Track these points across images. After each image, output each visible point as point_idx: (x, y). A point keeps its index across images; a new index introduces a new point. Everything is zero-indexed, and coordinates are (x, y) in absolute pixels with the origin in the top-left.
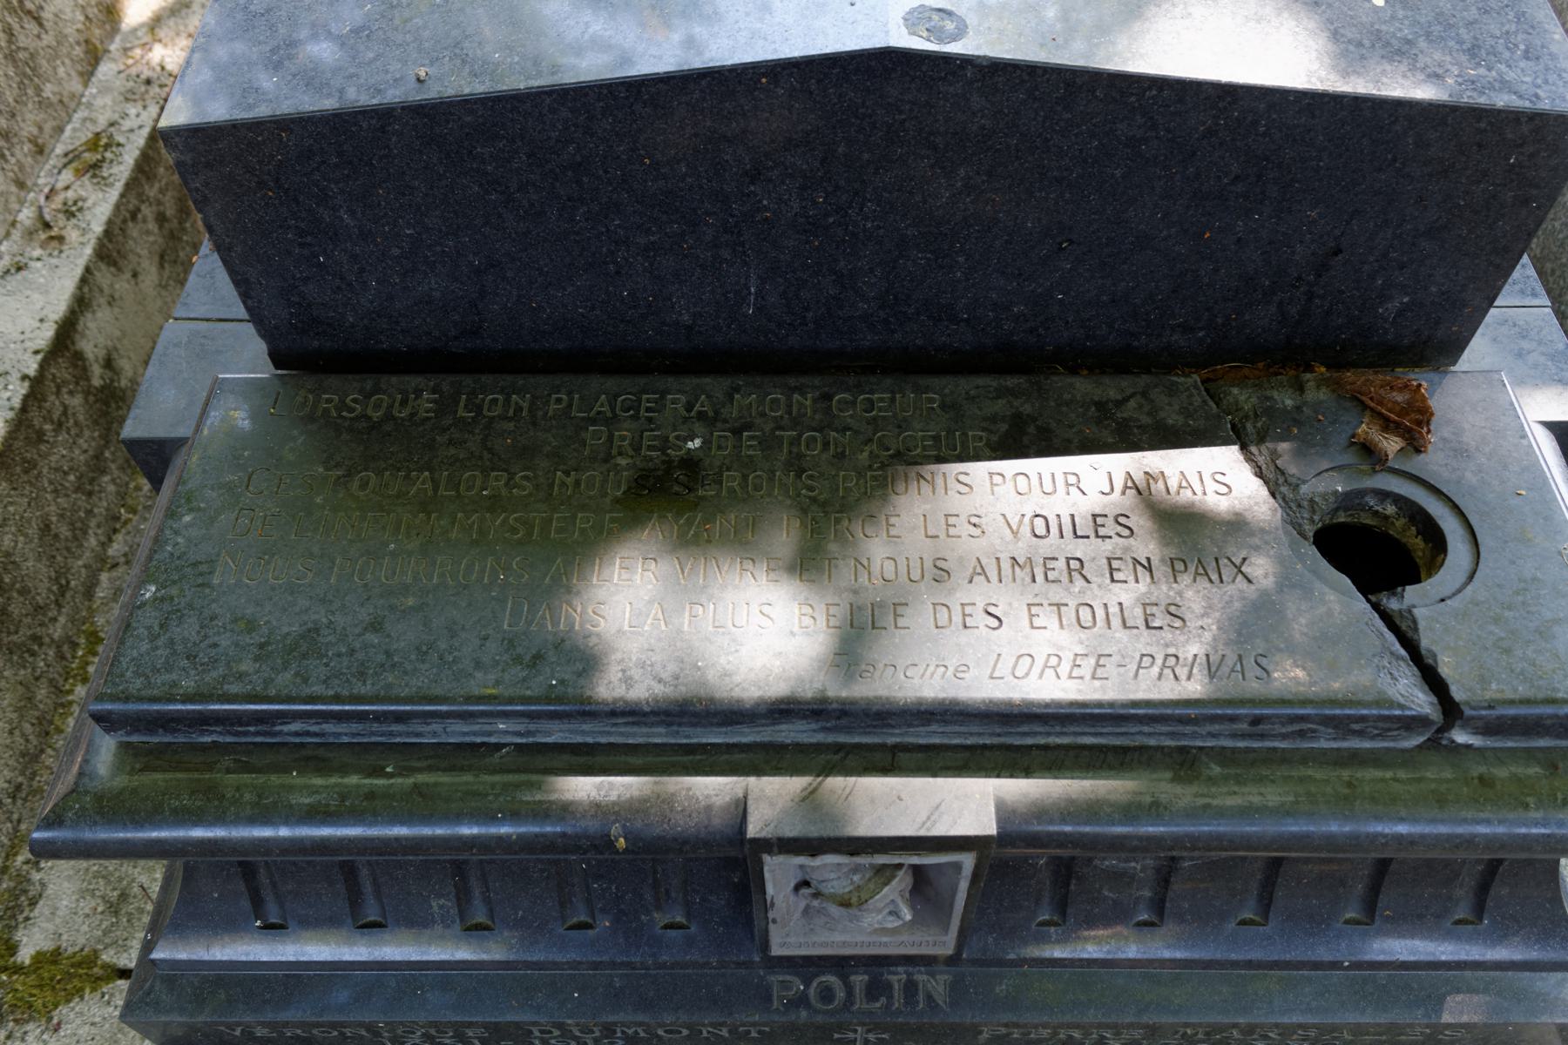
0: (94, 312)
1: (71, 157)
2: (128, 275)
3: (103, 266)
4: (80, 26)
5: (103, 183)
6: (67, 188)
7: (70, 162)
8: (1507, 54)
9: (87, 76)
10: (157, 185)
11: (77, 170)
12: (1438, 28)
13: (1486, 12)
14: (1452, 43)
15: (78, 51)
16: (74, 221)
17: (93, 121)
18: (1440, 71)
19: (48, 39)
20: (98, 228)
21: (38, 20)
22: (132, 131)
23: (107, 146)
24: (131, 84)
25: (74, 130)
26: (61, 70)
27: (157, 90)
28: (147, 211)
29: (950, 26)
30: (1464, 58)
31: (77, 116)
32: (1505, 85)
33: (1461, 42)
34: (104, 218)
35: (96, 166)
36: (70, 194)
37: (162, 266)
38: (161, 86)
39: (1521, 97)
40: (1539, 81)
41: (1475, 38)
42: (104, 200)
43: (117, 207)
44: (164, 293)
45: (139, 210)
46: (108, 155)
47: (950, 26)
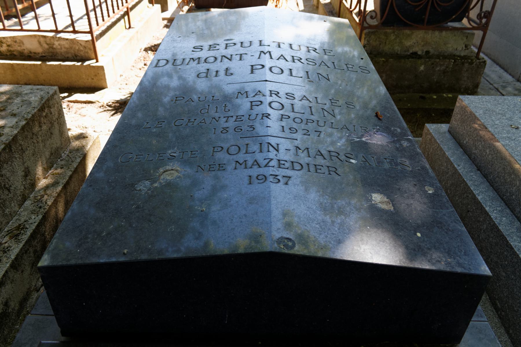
0: (5, 286)
1: (9, 232)
2: (20, 272)
3: (12, 270)
4: (22, 190)
5: (18, 241)
6: (6, 243)
7: (9, 234)
8: (459, 254)
9: (20, 206)
10: (36, 241)
11: (10, 236)
12: (437, 244)
13: (451, 239)
14: (442, 250)
15: (20, 198)
16: (6, 254)
17: (20, 220)
18: (440, 260)
19: (10, 195)
20: (13, 257)
21: (9, 190)
22: (32, 223)
23: (22, 229)
24: (35, 208)
25: (13, 223)
26: (13, 205)
27: (43, 210)
28: (31, 250)
29: (290, 244)
30: (446, 255)
31: (16, 218)
32: (460, 265)
33: (445, 249)
34: (16, 254)
35: (17, 235)
36: (6, 245)
37: (32, 267)
38: (44, 209)
39: (465, 269)
40: (470, 263)
41: (449, 248)
42: (17, 247)
43: (21, 249)
44: (31, 277)
45: (28, 249)
46: (22, 232)
47: (290, 244)
